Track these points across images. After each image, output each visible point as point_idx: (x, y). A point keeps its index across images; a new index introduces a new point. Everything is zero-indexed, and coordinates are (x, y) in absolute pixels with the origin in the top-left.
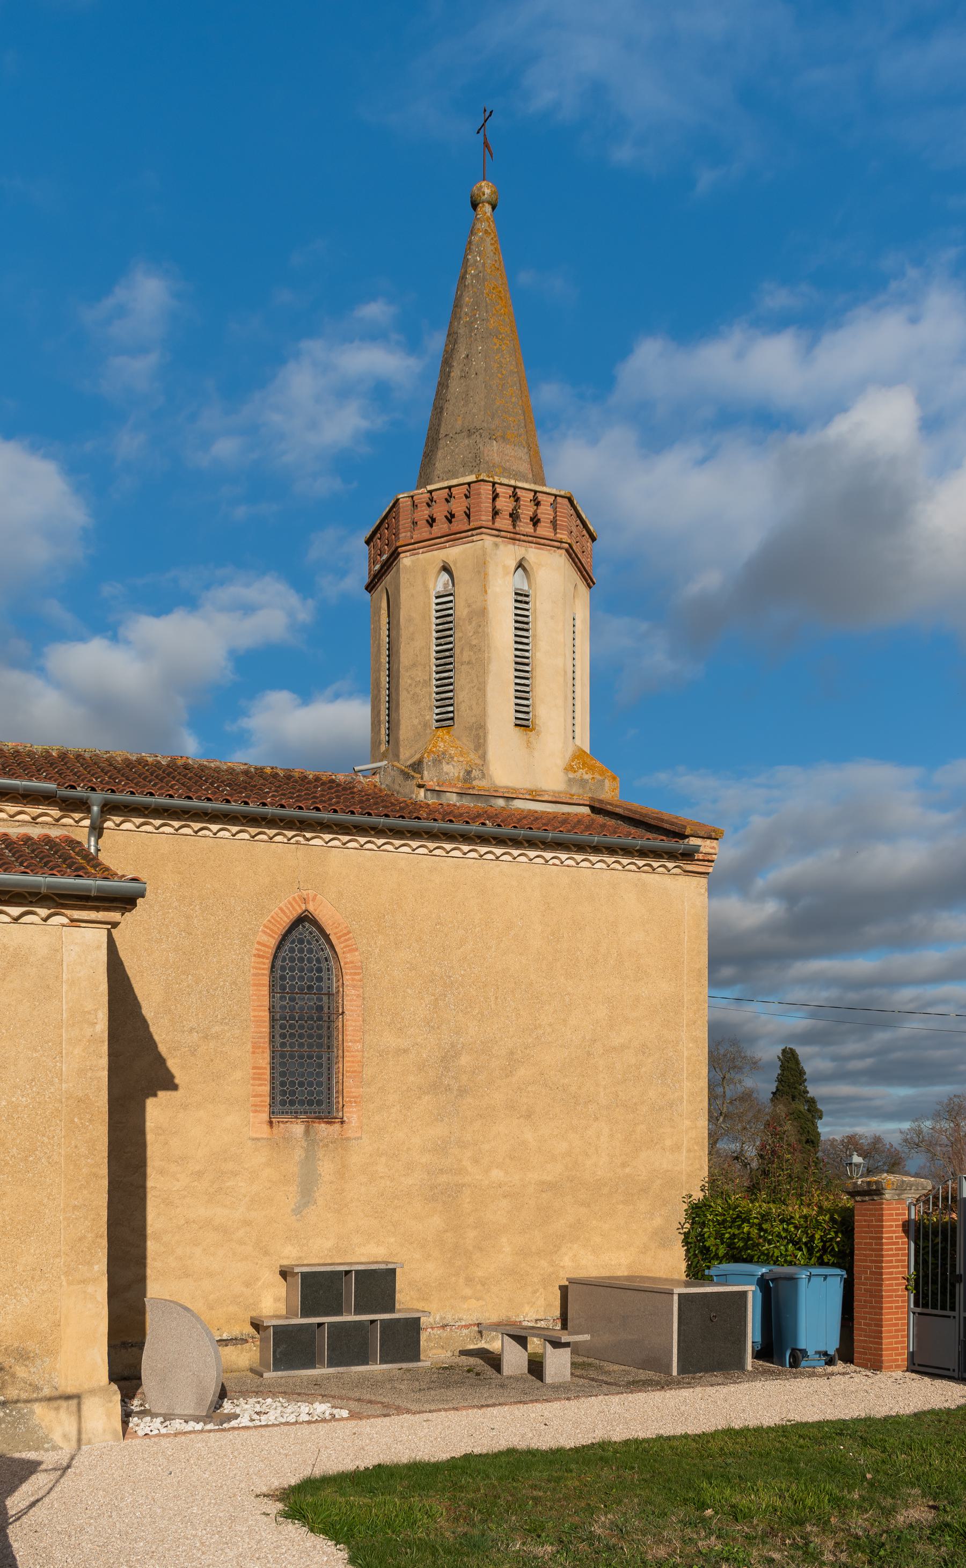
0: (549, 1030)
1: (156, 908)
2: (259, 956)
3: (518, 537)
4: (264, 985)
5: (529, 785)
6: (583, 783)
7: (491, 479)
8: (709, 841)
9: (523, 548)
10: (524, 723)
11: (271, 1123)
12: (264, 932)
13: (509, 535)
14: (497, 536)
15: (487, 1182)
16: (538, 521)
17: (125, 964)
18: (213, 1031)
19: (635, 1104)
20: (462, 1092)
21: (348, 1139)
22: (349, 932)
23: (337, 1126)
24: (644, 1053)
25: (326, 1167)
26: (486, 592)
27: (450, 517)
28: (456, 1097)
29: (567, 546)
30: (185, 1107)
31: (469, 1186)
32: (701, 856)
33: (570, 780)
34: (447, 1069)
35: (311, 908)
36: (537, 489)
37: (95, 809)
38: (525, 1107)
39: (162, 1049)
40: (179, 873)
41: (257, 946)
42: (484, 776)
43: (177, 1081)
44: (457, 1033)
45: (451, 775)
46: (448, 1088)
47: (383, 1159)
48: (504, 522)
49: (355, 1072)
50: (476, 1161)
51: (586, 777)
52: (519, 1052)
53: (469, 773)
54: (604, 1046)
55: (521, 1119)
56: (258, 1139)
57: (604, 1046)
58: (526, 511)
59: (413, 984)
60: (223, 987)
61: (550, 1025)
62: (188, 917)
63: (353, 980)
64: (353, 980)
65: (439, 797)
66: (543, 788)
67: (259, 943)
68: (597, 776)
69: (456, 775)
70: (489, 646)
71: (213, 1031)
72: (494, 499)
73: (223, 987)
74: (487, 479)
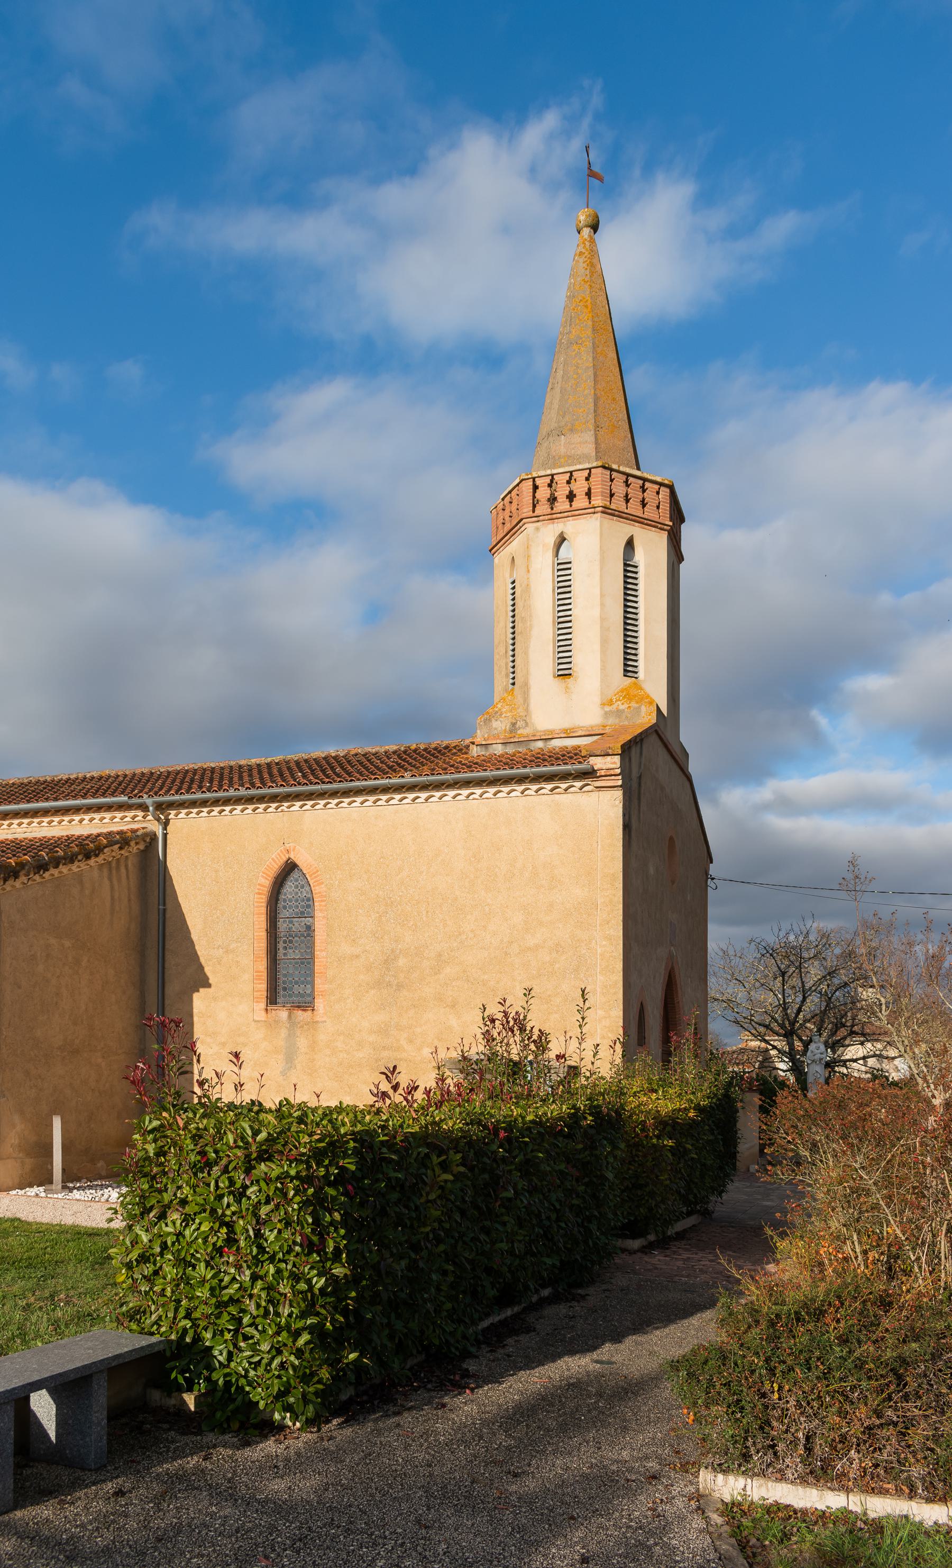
0: (471, 935)
1: (199, 868)
2: (259, 894)
3: (554, 516)
4: (262, 914)
5: (566, 725)
6: (619, 713)
7: (530, 476)
8: (609, 758)
9: (562, 524)
10: (564, 673)
11: (267, 1010)
12: (262, 876)
13: (546, 517)
14: (538, 521)
15: (419, 1058)
16: (568, 497)
17: (182, 906)
18: (231, 947)
19: (549, 996)
20: (400, 987)
21: (317, 1022)
22: (318, 871)
23: (309, 1013)
24: (557, 952)
25: (302, 1043)
26: (528, 571)
27: (571, 497)
28: (395, 991)
29: (600, 509)
30: (215, 999)
31: (406, 1060)
32: (603, 773)
33: (606, 713)
34: (388, 969)
35: (292, 857)
36: (571, 470)
37: (151, 808)
38: (451, 998)
39: (202, 960)
40: (211, 842)
41: (258, 887)
42: (527, 724)
43: (210, 981)
44: (396, 941)
45: (500, 729)
46: (389, 984)
47: (342, 1038)
48: (543, 508)
49: (321, 973)
50: (411, 1041)
51: (621, 707)
52: (446, 954)
53: (514, 724)
54: (520, 946)
55: (447, 1009)
56: (258, 1021)
57: (520, 946)
58: (562, 493)
59: (363, 905)
60: (237, 917)
61: (472, 931)
62: (217, 871)
63: (320, 905)
64: (320, 905)
65: (487, 748)
66: (581, 725)
67: (259, 884)
68: (634, 704)
69: (504, 728)
70: (531, 616)
71: (231, 947)
72: (534, 492)
73: (237, 917)
74: (526, 477)
